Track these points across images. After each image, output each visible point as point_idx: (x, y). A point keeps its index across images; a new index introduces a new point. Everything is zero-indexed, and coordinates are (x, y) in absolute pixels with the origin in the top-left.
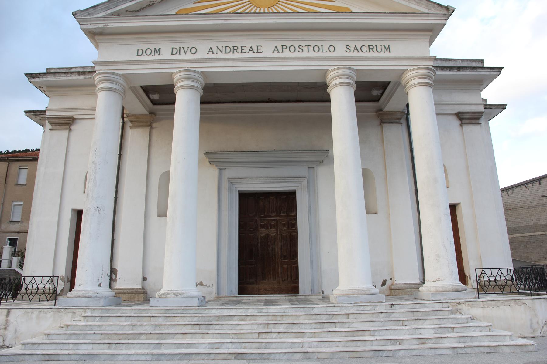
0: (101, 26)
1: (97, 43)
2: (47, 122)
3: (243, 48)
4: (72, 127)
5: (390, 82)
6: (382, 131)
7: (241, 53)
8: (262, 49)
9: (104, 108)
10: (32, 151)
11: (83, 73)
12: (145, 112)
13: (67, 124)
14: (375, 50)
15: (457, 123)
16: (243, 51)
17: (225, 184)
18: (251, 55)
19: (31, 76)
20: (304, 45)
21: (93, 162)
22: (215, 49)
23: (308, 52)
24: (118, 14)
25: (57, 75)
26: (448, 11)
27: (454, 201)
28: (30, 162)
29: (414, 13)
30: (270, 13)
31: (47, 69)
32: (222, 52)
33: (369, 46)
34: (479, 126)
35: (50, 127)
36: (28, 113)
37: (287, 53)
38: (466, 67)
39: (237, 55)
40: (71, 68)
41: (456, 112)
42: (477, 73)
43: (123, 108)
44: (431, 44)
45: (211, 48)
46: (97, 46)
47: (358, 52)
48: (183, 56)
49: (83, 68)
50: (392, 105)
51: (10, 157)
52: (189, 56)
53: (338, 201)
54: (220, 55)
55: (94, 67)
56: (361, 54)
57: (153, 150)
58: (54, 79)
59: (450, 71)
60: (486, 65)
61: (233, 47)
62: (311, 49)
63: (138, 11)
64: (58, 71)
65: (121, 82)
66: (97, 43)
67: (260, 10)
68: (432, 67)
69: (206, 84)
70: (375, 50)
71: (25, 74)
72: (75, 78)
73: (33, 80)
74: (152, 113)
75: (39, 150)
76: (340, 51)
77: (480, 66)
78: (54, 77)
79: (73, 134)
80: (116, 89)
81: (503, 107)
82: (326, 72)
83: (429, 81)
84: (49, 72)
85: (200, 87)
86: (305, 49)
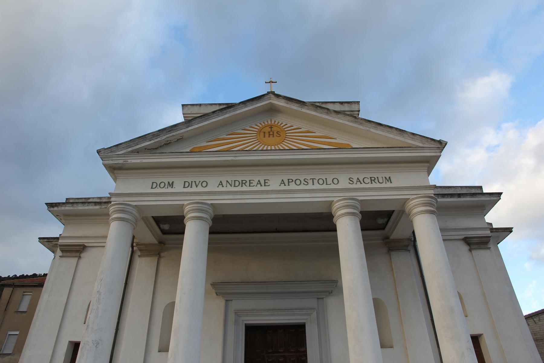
0: (121, 162)
1: (115, 176)
2: (58, 249)
3: (251, 182)
4: (82, 255)
5: (394, 211)
6: (391, 259)
7: (250, 186)
8: (269, 183)
9: (115, 236)
10: (40, 276)
11: (100, 203)
12: (154, 241)
13: (77, 251)
14: (376, 181)
15: (465, 248)
16: (251, 185)
17: (232, 317)
18: (259, 188)
19: (51, 205)
20: (308, 178)
21: (98, 292)
22: (224, 183)
23: (313, 184)
24: (138, 152)
25: (75, 205)
26: (441, 145)
27: (476, 332)
28: (36, 288)
29: (410, 147)
30: (276, 150)
31: (67, 199)
32: (231, 186)
33: (371, 178)
34: (489, 251)
35: (61, 254)
36: (43, 240)
37: (293, 186)
38: (466, 194)
39: (245, 188)
40: (89, 198)
41: (463, 237)
42: (479, 200)
43: (134, 237)
44: (429, 176)
45: (221, 182)
46: (115, 180)
47: (361, 183)
48: (194, 189)
49: (100, 198)
50: (399, 233)
51: (16, 282)
52: (200, 189)
53: (350, 335)
54: (230, 189)
55: (110, 198)
56: (364, 186)
57: (160, 279)
58: (72, 208)
59: (451, 197)
60: (485, 191)
61: (242, 181)
62: (316, 182)
63: (156, 149)
64: (77, 201)
65: (134, 212)
66: (115, 176)
67: (267, 148)
68: (433, 195)
69: (215, 215)
70: (376, 181)
71: (46, 204)
72: (91, 207)
73: (52, 209)
74: (161, 242)
75: (47, 274)
76: (344, 183)
77: (480, 192)
78: (72, 206)
79: (81, 261)
80: (129, 219)
81: (509, 230)
82: (331, 203)
83: (432, 209)
84: (68, 202)
85: (209, 218)
86: (310, 182)
